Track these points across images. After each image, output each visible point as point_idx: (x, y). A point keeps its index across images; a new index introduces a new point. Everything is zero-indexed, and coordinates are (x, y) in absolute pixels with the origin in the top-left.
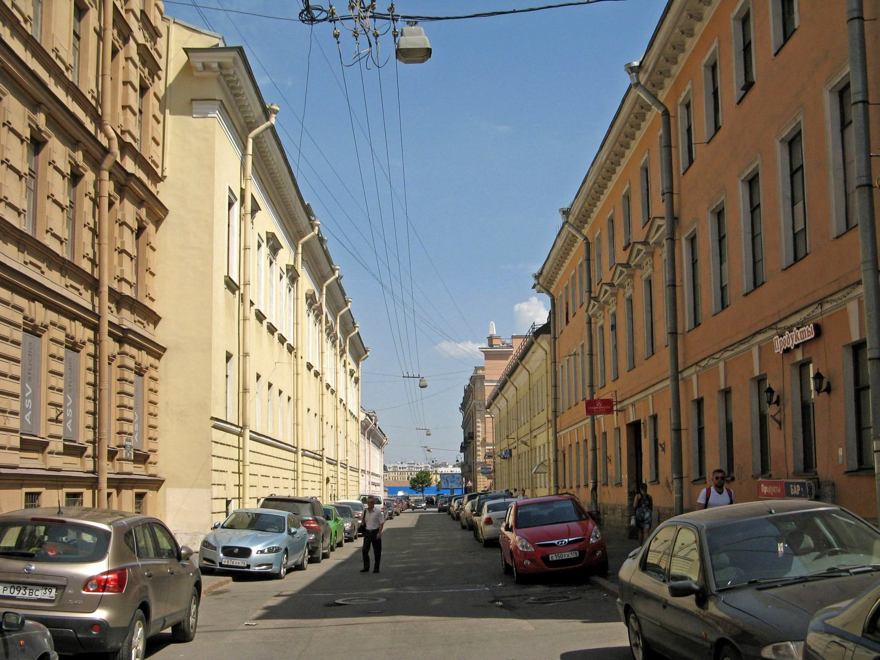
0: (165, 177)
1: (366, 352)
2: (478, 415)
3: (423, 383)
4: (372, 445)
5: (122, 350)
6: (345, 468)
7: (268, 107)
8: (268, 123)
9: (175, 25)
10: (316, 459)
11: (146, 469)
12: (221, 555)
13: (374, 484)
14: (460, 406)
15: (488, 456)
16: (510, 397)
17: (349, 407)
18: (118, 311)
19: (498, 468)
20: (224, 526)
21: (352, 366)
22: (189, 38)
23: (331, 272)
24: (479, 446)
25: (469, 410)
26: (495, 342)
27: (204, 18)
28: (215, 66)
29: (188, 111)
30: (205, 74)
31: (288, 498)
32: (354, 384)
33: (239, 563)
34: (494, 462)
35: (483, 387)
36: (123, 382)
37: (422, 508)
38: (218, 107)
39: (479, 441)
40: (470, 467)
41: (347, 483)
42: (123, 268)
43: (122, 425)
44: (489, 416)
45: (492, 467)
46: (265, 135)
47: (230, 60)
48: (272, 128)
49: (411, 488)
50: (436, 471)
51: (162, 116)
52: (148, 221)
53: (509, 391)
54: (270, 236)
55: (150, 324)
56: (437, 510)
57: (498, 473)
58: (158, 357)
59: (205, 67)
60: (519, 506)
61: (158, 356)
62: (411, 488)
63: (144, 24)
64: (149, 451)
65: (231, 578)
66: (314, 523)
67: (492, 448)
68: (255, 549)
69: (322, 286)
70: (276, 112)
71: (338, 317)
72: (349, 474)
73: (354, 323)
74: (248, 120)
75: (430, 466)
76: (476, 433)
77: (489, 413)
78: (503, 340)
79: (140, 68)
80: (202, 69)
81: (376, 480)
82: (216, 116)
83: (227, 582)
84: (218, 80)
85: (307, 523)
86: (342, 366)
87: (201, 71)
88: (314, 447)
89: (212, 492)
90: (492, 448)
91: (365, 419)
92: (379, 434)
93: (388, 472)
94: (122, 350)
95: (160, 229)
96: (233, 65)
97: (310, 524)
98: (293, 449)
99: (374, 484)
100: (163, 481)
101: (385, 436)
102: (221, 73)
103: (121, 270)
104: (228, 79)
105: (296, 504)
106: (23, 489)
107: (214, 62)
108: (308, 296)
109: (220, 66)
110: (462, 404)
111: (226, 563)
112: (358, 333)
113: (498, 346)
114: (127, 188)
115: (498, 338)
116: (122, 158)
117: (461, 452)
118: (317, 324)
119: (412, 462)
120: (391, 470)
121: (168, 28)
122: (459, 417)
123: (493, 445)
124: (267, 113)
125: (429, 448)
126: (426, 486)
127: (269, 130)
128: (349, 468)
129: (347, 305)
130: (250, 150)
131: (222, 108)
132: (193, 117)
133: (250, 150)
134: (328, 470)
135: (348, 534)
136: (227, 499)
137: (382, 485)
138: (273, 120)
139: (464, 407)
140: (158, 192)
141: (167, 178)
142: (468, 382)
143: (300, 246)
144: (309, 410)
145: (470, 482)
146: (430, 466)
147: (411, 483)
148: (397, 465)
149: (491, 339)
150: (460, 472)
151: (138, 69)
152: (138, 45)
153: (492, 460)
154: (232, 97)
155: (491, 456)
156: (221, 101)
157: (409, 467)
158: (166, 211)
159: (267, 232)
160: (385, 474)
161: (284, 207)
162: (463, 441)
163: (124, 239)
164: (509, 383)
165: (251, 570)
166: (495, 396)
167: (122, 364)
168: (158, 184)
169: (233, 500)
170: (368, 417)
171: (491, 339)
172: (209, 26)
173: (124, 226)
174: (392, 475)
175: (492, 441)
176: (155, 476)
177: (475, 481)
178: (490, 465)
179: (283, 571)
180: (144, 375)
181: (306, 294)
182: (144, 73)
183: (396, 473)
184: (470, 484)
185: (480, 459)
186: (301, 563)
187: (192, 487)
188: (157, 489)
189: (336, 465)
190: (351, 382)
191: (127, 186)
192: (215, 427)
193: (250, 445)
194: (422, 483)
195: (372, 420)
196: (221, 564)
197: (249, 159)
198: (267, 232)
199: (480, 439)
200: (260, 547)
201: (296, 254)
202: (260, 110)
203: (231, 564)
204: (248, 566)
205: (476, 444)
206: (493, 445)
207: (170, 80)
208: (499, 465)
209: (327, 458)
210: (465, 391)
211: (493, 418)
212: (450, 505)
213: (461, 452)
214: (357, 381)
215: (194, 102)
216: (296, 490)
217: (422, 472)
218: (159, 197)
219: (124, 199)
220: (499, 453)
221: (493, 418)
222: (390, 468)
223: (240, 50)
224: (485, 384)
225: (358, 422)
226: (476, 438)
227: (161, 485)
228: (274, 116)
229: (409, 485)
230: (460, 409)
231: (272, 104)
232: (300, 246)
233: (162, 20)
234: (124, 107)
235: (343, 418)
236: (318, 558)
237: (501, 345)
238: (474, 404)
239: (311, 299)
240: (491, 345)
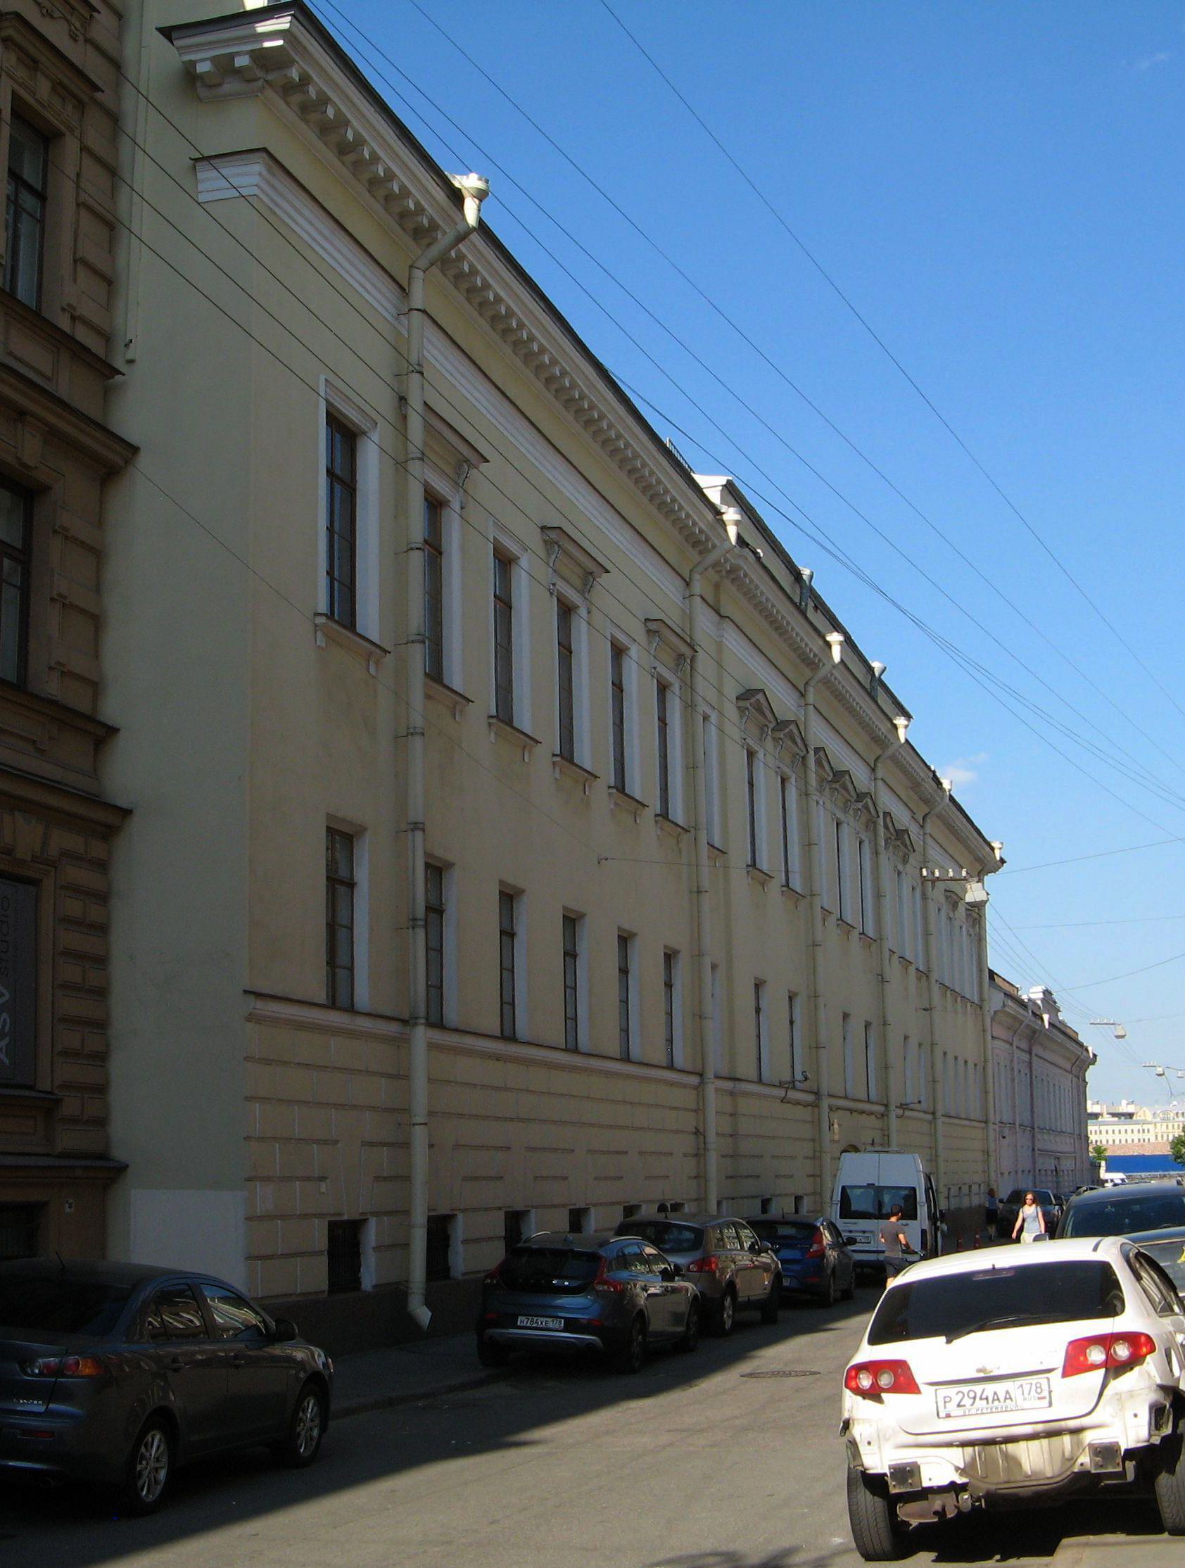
215: (199, 166)
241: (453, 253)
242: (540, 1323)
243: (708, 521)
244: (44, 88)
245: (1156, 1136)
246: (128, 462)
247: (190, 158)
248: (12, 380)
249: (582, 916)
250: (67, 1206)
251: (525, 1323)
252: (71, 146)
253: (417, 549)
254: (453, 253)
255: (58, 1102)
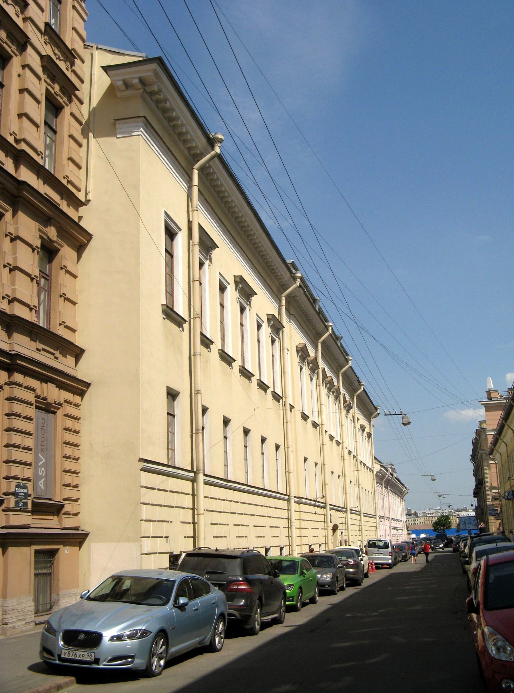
0: (89, 201)
1: (376, 409)
2: (485, 463)
3: (405, 421)
4: (391, 494)
5: (11, 379)
6: (359, 515)
7: (212, 137)
8: (213, 153)
9: (99, 50)
10: (318, 506)
11: (60, 522)
12: (61, 643)
13: (394, 528)
14: (470, 458)
15: (495, 499)
16: (509, 441)
17: (360, 458)
18: (9, 337)
19: (504, 509)
20: (91, 596)
21: (363, 421)
22: (112, 61)
23: (325, 329)
24: (488, 490)
25: (477, 460)
26: (493, 395)
27: (135, 47)
28: (136, 81)
29: (112, 131)
30: (128, 93)
31: (215, 553)
32: (367, 439)
33: (83, 656)
34: (501, 504)
35: (486, 435)
36: (13, 417)
37: (440, 548)
38: (142, 124)
39: (488, 486)
40: (482, 510)
41: (362, 529)
42: (16, 287)
43: (9, 468)
44: (493, 462)
45: (498, 508)
46: (211, 164)
47: (151, 74)
48: (219, 157)
49: (433, 531)
50: (458, 515)
51: (86, 140)
52: (60, 241)
53: (507, 435)
54: (238, 279)
55: (68, 356)
56: (451, 549)
57: (505, 514)
58: (82, 394)
59: (127, 85)
60: (494, 565)
61: (80, 392)
62: (433, 531)
63: (50, 38)
64: (64, 500)
65: (73, 678)
66: (244, 585)
67: (497, 491)
68: (107, 634)
69: (317, 343)
70: (221, 141)
71: (341, 374)
72: (362, 520)
73: (359, 382)
74: (193, 152)
75: (453, 511)
76: (484, 479)
77: (493, 460)
78: (501, 394)
79: (45, 81)
80: (124, 88)
81: (398, 525)
82: (140, 133)
83: (67, 685)
84: (144, 99)
85: (236, 585)
86: (349, 421)
87: (124, 91)
88: (314, 493)
89: (141, 547)
90: (497, 491)
91: (381, 470)
92: (397, 483)
93: (419, 517)
94: (11, 379)
95: (85, 255)
96: (157, 81)
97: (238, 585)
98: (287, 497)
99: (394, 528)
100: (86, 535)
101: (404, 486)
102: (144, 90)
103: (13, 289)
104: (155, 98)
105: (222, 560)
106: (32, 546)
107: (133, 78)
108: (299, 349)
109: (142, 81)
110: (472, 456)
111: (66, 656)
112: (364, 390)
113: (496, 399)
114: (21, 199)
115: (496, 391)
116: (17, 168)
117: (474, 497)
118: (314, 378)
119: (438, 508)
120: (421, 516)
121: (92, 55)
122: (471, 467)
123: (498, 488)
124: (211, 142)
125: (440, 494)
126: (447, 528)
127: (216, 159)
128: (362, 515)
129: (348, 362)
130: (196, 180)
131: (147, 124)
132: (117, 138)
133: (196, 180)
134: (337, 518)
135: (329, 586)
136: (266, 547)
137: (405, 529)
138: (217, 150)
139: (474, 457)
140: (80, 218)
141: (90, 203)
142: (474, 436)
143: (283, 299)
144: (306, 459)
145: (482, 524)
146: (453, 511)
147: (434, 526)
148: (425, 511)
149: (489, 392)
150: (475, 515)
151: (43, 80)
152: (42, 57)
153: (498, 502)
154: (166, 122)
155: (497, 499)
156: (145, 117)
157: (435, 512)
158: (89, 236)
159: (234, 276)
160: (407, 520)
161: (259, 257)
162: (475, 487)
163: (18, 255)
164: (506, 427)
165: (101, 666)
166: (495, 442)
167: (11, 395)
168: (80, 208)
169: (312, 545)
170: (383, 469)
171: (489, 392)
172: (137, 49)
173: (18, 240)
174: (422, 519)
175: (497, 485)
176: (77, 529)
177: (487, 522)
178: (497, 507)
179: (157, 663)
180: (56, 412)
181: (296, 347)
182: (53, 89)
183: (426, 518)
184: (482, 525)
185: (489, 502)
186: (211, 642)
187: (118, 541)
188: (80, 544)
189: (346, 512)
190: (362, 438)
191: (20, 197)
192: (144, 470)
193: (203, 489)
194: (444, 525)
195: (387, 471)
196: (60, 659)
197: (195, 190)
198: (234, 276)
199: (488, 484)
200: (114, 631)
201: (280, 306)
202: (203, 140)
203: (73, 657)
204: (97, 661)
205: (485, 489)
206: (498, 488)
207: (95, 103)
208: (505, 506)
209: (330, 505)
210: (473, 443)
211: (496, 463)
212: (459, 546)
213: (474, 497)
214: (369, 435)
215: (117, 122)
216: (361, 536)
217: (443, 516)
218: (82, 224)
219: (17, 212)
220: (504, 495)
221: (496, 463)
222: (420, 514)
223: (160, 61)
224: (487, 433)
225: (373, 472)
226: (485, 483)
227: (84, 540)
228: (219, 145)
229: (432, 528)
230: (471, 460)
231: (216, 134)
232: (283, 299)
233: (85, 48)
234: (20, 116)
235: (354, 468)
236: (253, 628)
237: (499, 397)
238: (481, 453)
239: (302, 352)
240: (490, 398)
241: (207, 165)
242: (78, 656)
243: (169, 102)
244: (57, 87)
245: (420, 522)
246: (89, 241)
247: (114, 119)
248: (48, 204)
249: (230, 420)
250: (66, 550)
251: (71, 656)
252: (67, 111)
253: (197, 280)
254: (207, 165)
255: (63, 506)
